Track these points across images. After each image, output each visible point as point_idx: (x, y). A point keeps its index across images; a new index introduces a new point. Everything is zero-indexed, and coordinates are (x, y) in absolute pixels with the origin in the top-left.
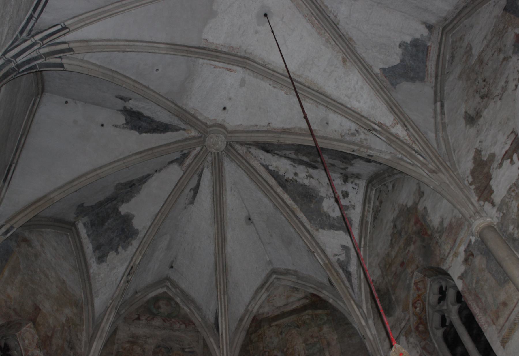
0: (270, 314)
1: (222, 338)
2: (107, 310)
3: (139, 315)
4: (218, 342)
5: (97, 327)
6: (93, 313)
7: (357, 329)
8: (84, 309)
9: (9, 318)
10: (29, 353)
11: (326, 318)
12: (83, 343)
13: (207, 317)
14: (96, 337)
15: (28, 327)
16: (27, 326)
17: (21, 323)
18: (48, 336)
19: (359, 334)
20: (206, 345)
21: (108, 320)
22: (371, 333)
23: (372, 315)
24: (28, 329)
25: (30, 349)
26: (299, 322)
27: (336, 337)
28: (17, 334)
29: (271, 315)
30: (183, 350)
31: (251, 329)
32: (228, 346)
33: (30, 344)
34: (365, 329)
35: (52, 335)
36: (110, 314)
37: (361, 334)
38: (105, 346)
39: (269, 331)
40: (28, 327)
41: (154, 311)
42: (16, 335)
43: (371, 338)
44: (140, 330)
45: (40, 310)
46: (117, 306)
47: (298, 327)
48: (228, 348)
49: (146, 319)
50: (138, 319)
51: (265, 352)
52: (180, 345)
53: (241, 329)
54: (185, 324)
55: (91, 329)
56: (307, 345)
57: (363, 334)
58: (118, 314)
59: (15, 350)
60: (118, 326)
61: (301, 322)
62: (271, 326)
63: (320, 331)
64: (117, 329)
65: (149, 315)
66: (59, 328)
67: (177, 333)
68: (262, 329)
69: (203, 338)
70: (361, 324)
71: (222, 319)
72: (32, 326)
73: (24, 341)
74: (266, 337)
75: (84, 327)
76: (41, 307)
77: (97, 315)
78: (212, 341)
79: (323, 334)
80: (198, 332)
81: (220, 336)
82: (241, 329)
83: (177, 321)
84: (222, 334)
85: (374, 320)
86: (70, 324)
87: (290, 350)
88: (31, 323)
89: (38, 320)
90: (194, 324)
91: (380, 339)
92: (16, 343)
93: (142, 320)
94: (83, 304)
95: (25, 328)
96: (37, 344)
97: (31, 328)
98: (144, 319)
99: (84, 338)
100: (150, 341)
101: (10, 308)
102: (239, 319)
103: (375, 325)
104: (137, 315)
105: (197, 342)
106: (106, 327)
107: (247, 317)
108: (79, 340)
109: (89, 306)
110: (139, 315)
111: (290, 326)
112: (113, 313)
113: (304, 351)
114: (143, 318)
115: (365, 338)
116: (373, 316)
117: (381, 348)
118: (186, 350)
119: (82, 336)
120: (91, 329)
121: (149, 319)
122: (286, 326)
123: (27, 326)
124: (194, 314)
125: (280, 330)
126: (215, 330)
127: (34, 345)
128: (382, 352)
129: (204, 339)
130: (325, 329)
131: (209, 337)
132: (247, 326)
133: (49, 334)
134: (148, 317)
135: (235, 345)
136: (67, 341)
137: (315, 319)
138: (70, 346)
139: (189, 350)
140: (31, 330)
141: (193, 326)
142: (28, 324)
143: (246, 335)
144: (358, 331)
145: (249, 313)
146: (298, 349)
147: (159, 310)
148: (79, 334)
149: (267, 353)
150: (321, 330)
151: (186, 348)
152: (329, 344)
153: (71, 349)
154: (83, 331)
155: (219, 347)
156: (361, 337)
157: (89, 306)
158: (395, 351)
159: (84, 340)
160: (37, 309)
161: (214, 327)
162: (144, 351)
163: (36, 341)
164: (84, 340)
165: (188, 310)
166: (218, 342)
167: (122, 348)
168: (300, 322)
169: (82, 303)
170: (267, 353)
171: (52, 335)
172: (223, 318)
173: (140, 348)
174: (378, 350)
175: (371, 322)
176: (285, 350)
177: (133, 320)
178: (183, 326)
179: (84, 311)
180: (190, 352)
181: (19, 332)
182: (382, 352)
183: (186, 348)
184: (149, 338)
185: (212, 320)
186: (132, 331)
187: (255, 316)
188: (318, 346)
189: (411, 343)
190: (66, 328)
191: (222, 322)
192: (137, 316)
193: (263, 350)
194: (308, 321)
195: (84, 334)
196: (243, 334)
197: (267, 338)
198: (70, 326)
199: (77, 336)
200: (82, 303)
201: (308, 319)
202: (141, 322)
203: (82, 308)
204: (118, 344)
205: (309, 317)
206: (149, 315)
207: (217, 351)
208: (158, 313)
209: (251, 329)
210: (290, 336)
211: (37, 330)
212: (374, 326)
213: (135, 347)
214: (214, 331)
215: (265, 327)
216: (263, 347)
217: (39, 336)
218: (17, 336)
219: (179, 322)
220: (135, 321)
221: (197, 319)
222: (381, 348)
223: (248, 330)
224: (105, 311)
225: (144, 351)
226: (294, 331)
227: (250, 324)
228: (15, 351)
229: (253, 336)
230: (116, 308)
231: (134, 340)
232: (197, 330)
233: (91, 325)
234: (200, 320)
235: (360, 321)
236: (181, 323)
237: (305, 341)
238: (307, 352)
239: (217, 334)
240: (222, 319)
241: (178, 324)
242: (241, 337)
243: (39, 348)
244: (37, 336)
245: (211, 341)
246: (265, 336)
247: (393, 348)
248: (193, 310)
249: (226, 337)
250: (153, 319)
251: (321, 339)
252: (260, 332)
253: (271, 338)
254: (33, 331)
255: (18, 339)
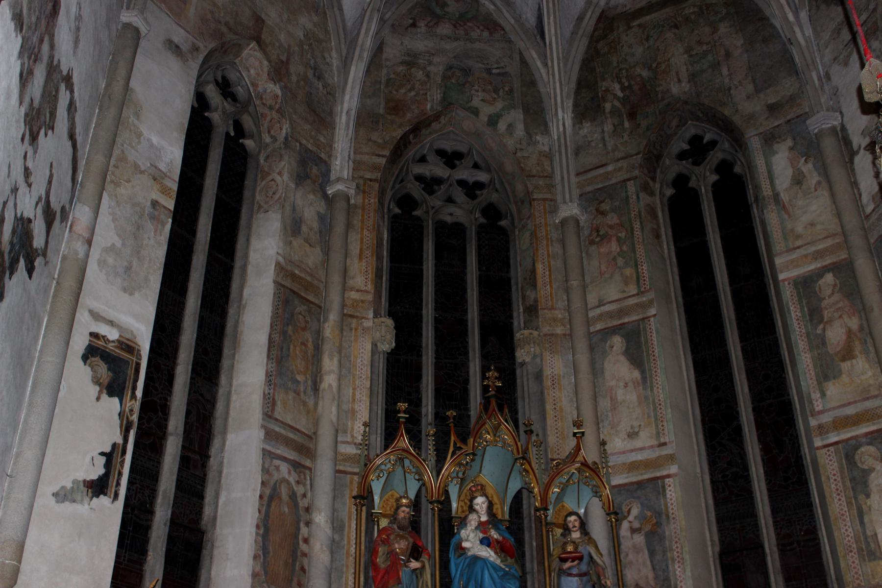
0: (628, 8)
1: (551, 49)
2: (365, 14)
3: (414, 19)
4: (544, 58)
5: (352, 44)
6: (343, 21)
7: (778, 27)
8: (328, 16)
9: (221, 38)
10: (259, 89)
11: (724, 11)
12: (335, 68)
13: (524, 16)
14: (352, 59)
15: (250, 50)
16: (249, 49)
17: (240, 45)
18: (282, 61)
19: (780, 37)
20: (524, 62)
21: (368, 30)
22: (804, 35)
23: (807, 4)
24: (251, 52)
25: (260, 83)
26: (678, 19)
27: (740, 42)
28: (237, 61)
29: (629, 9)
30: (489, 71)
31: (596, 34)
32: (561, 62)
33: (258, 74)
34: (792, 28)
35: (288, 59)
36: (370, 22)
37: (786, 37)
38: (368, 71)
39: (627, 35)
40: (250, 50)
41: (438, 11)
42: (235, 63)
43: (803, 42)
44: (419, 43)
45: (263, 21)
46: (380, 7)
47: (676, 27)
48: (561, 65)
49: (426, 25)
50: (414, 25)
51: (621, 69)
52: (484, 64)
53: (580, 33)
54: (488, 29)
55: (343, 46)
56: (691, 56)
57: (788, 37)
58: (382, 21)
59: (239, 85)
60: (383, 39)
61: (681, 19)
62: (630, 28)
63: (713, 33)
64: (382, 43)
65: (429, 19)
66: (296, 48)
67: (477, 45)
68: (615, 33)
69: (520, 50)
70: (786, 18)
71: (549, 19)
72: (257, 47)
73: (249, 71)
74: (623, 46)
75: (333, 44)
76: (263, 16)
77: (349, 24)
78: (535, 56)
79: (720, 37)
80: (510, 41)
81: (548, 47)
82: (580, 33)
83: (476, 26)
84: (551, 44)
85: (809, 11)
86: (311, 41)
87: (663, 67)
88: (255, 42)
89: (263, 37)
90: (503, 30)
91: (818, 44)
92: (238, 74)
93: (421, 27)
94: (326, 7)
95: (246, 52)
96: (268, 75)
97: (255, 50)
98: (423, 25)
99: (335, 62)
100: (436, 59)
101: (220, 22)
102: (576, 17)
103: (810, 21)
104: (411, 19)
105: (509, 57)
106: (366, 41)
107: (589, 13)
108: (328, 64)
109: (336, 9)
110: (414, 19)
111: (663, 26)
112: (375, 20)
113: (685, 67)
114: (422, 24)
115: (792, 44)
116: (809, 6)
117: (818, 60)
118: (494, 71)
119: (331, 57)
120: (343, 46)
121: (431, 24)
122: (655, 27)
123: (249, 49)
124: (502, 12)
125: (646, 33)
126: (538, 37)
127: (265, 76)
128: (820, 67)
129: (521, 53)
130: (723, 29)
131: (528, 49)
132: (590, 29)
133: (284, 58)
134: (429, 22)
135: (571, 60)
136: (311, 67)
137: (705, 13)
138: (316, 74)
139: (498, 71)
140: (255, 53)
141: (502, 32)
142: (250, 45)
143: (589, 43)
144: (781, 32)
145: (592, 7)
146: (676, 64)
147: (446, 9)
148: (326, 55)
149: (624, 71)
150: (715, 30)
151: (493, 69)
152: (728, 55)
153: (319, 78)
154: (332, 50)
155: (546, 65)
156: (786, 40)
157: (336, 9)
158: (869, 70)
159: (335, 65)
160: (259, 21)
161: (536, 32)
162: (428, 76)
163: (266, 69)
164: (335, 65)
165: (493, 7)
166: (544, 58)
167: (394, 73)
168: (680, 19)
169: (324, 6)
170: (624, 71)
171: (288, 59)
172: (552, 18)
173: (421, 72)
174: (813, 63)
175: (804, 15)
176: (654, 65)
177: (407, 29)
178: (486, 34)
179: (328, 18)
180: (499, 74)
181: (239, 59)
182: (820, 67)
183: (493, 69)
184: (433, 54)
185: (532, 21)
186: (406, 46)
187: (603, 12)
188: (710, 58)
189: (874, 50)
190: (306, 47)
191: (549, 23)
192: (411, 21)
193: (618, 66)
194: (693, 17)
195: (334, 54)
196: (585, 41)
197: (624, 48)
198: (311, 44)
199: (325, 59)
200: (324, 6)
201: (694, 13)
202: (419, 30)
203: (325, 13)
204: (386, 67)
205: (696, 9)
206: (429, 19)
207: (543, 71)
208: (445, 15)
209: (596, 34)
210: (663, 42)
211: (265, 53)
212: (809, 22)
213: (413, 70)
214: (536, 39)
215: (621, 29)
216: (618, 63)
217: (270, 62)
218: (238, 64)
219: (479, 28)
220: (409, 28)
221: (507, 20)
222: (818, 60)
223: (592, 37)
224: (362, 16)
225: (428, 76)
226: (669, 35)
227: (595, 25)
228: (239, 88)
229: (600, 45)
230: (378, 11)
231: (411, 60)
232: (510, 38)
233: (343, 40)
234: (513, 21)
235: (785, 14)
236: (482, 28)
237: (688, 50)
238: (691, 68)
239: (542, 44)
240: (549, 19)
241: (478, 31)
242: (580, 48)
243: (273, 79)
244: (266, 63)
245: (533, 56)
246: (621, 44)
247: (867, 66)
248: (501, 6)
249: (557, 48)
250: (436, 24)
251: (715, 45)
252: (612, 38)
253: (630, 46)
254: (259, 54)
255: (240, 69)
